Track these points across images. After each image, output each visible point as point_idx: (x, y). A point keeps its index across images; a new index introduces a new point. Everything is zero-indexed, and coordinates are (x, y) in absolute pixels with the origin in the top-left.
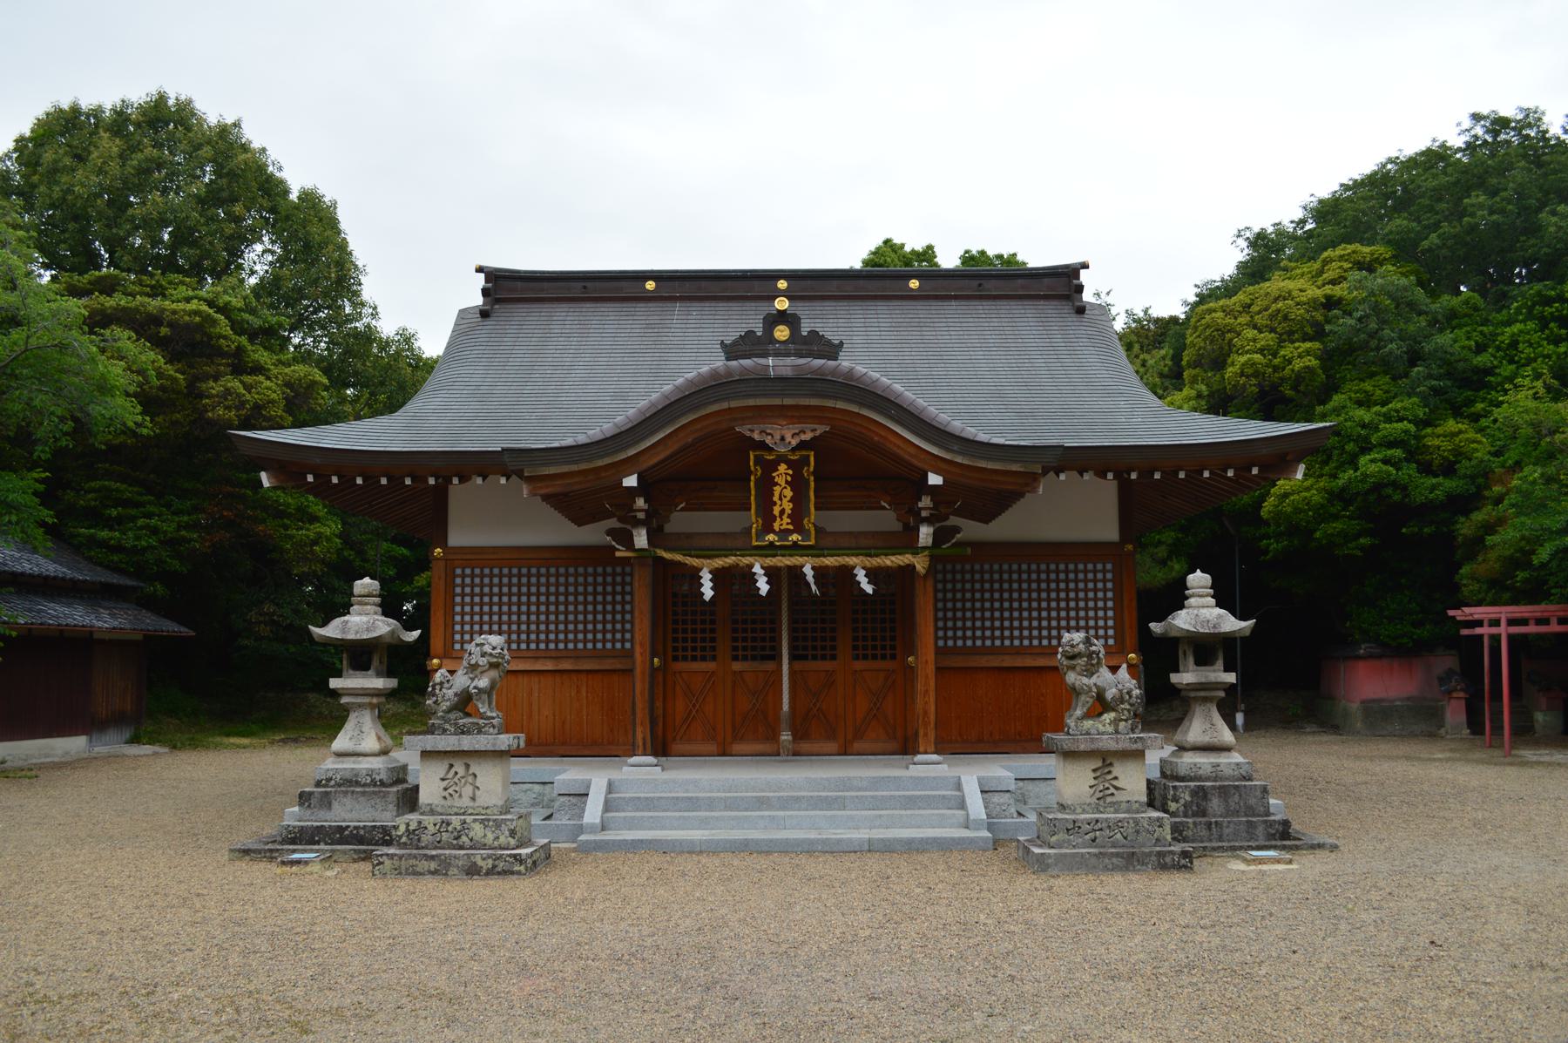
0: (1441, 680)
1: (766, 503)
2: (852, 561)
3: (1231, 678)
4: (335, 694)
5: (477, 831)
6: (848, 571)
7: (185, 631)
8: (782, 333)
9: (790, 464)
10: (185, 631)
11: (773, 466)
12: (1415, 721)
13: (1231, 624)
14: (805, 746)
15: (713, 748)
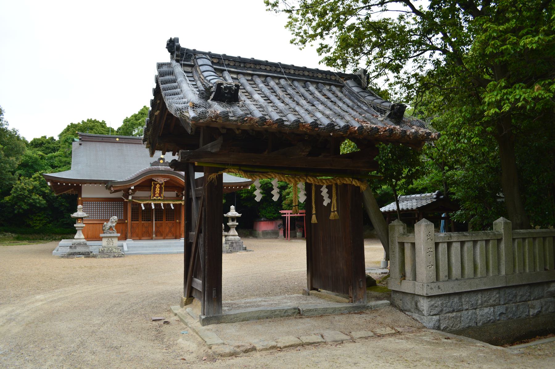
0: (279, 226)
1: (154, 191)
2: (170, 202)
3: (237, 224)
4: (75, 228)
5: (114, 250)
6: (169, 205)
7: (383, 209)
8: (161, 161)
9: (160, 184)
10: (383, 209)
11: (156, 184)
12: (274, 235)
13: (238, 215)
14: (157, 238)
15: (138, 238)
